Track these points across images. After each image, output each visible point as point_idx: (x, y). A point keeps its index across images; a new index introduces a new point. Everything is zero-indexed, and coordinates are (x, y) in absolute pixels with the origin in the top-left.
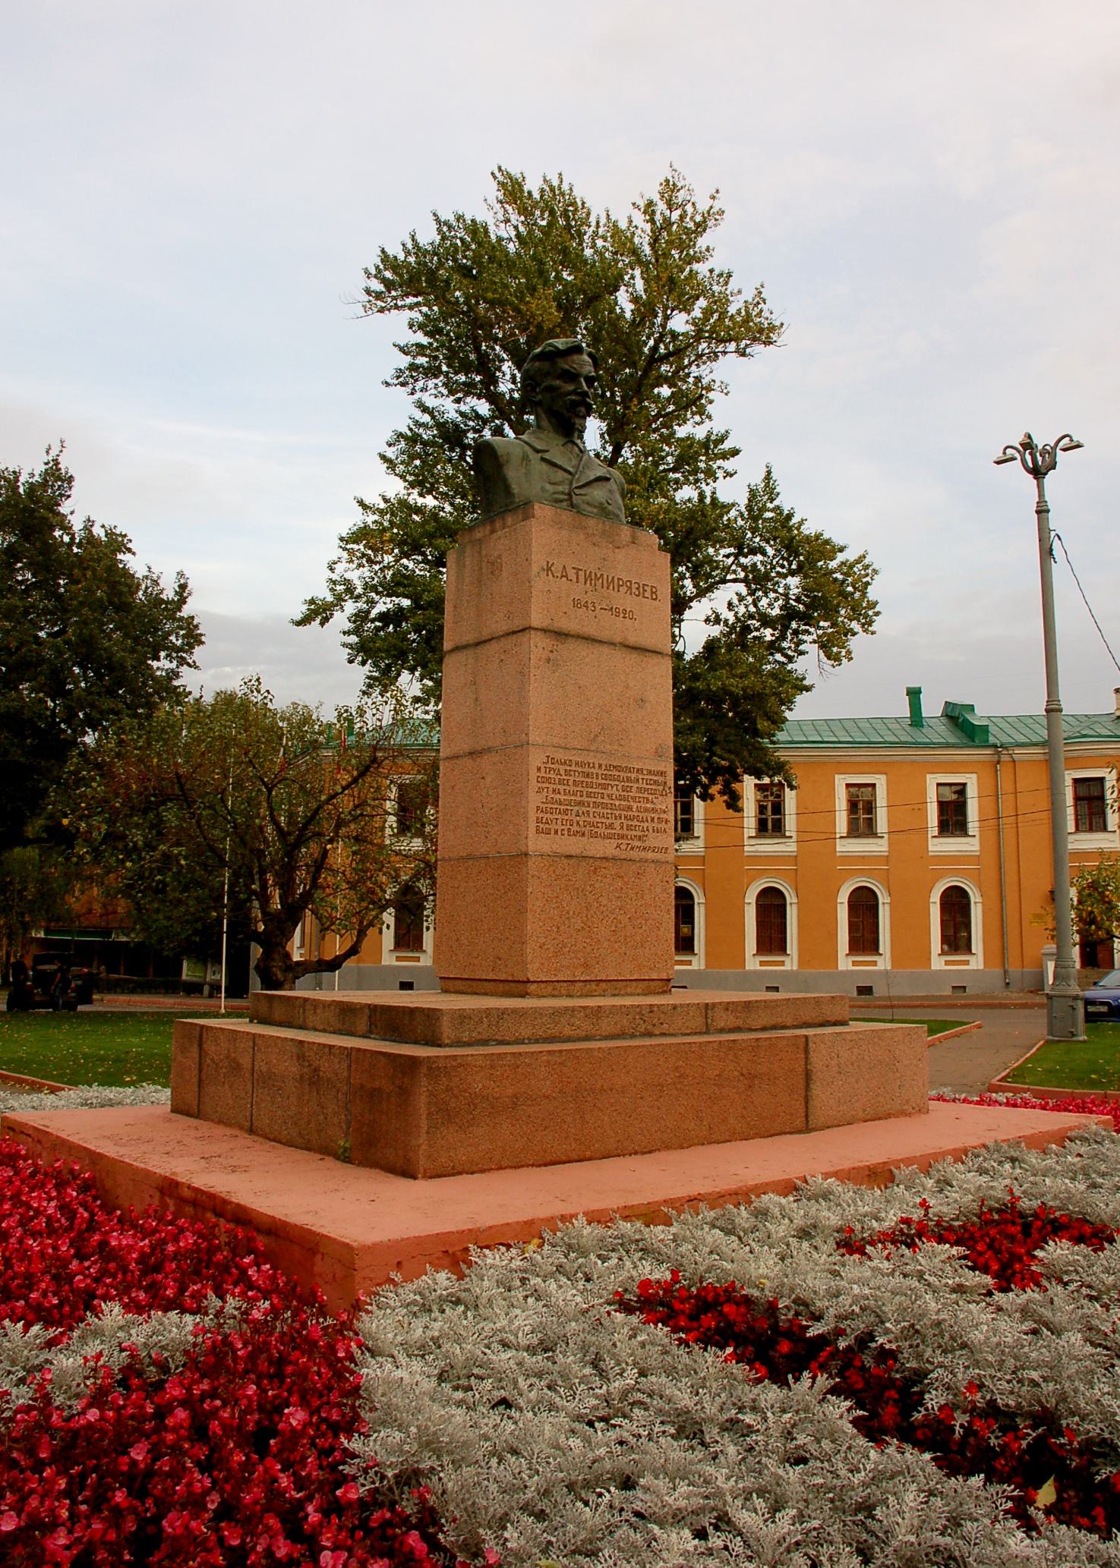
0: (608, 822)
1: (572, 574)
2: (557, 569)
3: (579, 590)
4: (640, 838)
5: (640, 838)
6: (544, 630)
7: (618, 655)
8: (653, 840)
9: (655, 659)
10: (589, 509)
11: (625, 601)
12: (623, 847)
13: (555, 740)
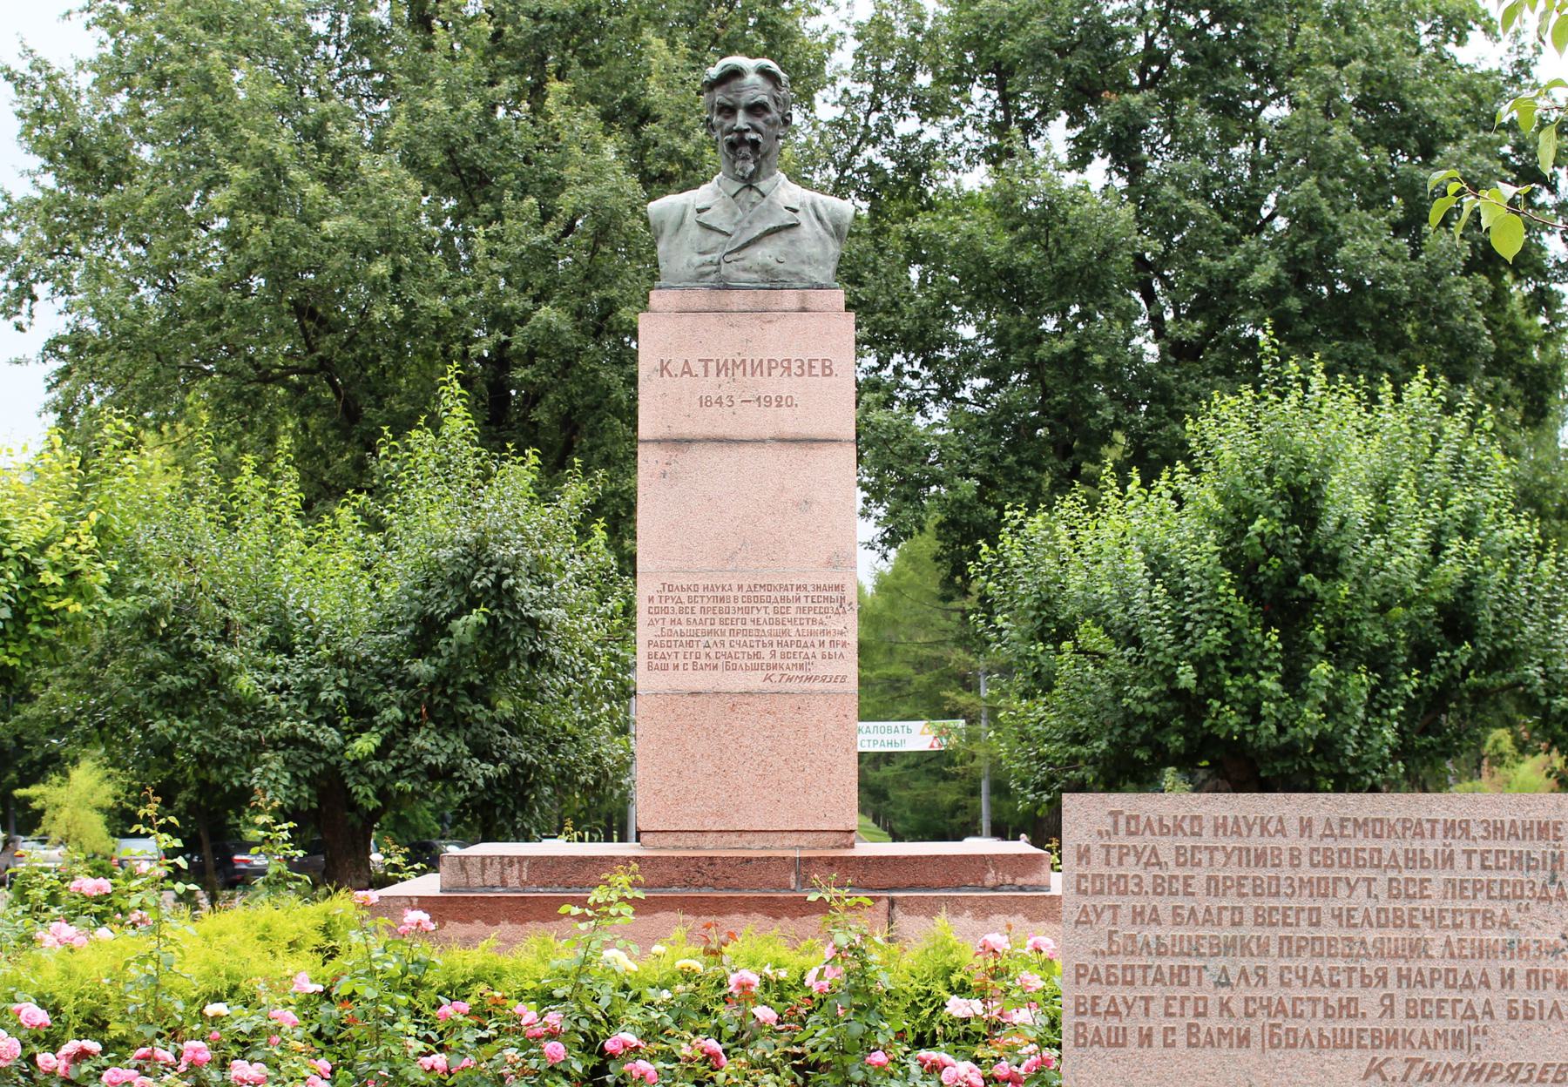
0: (1334, 997)
1: (698, 368)
2: (676, 366)
3: (710, 385)
4: (1457, 1040)
5: (1457, 1040)
6: (658, 441)
7: (769, 457)
8: (821, 668)
9: (828, 449)
10: (745, 276)
11: (776, 384)
12: (776, 678)
13: (674, 565)
